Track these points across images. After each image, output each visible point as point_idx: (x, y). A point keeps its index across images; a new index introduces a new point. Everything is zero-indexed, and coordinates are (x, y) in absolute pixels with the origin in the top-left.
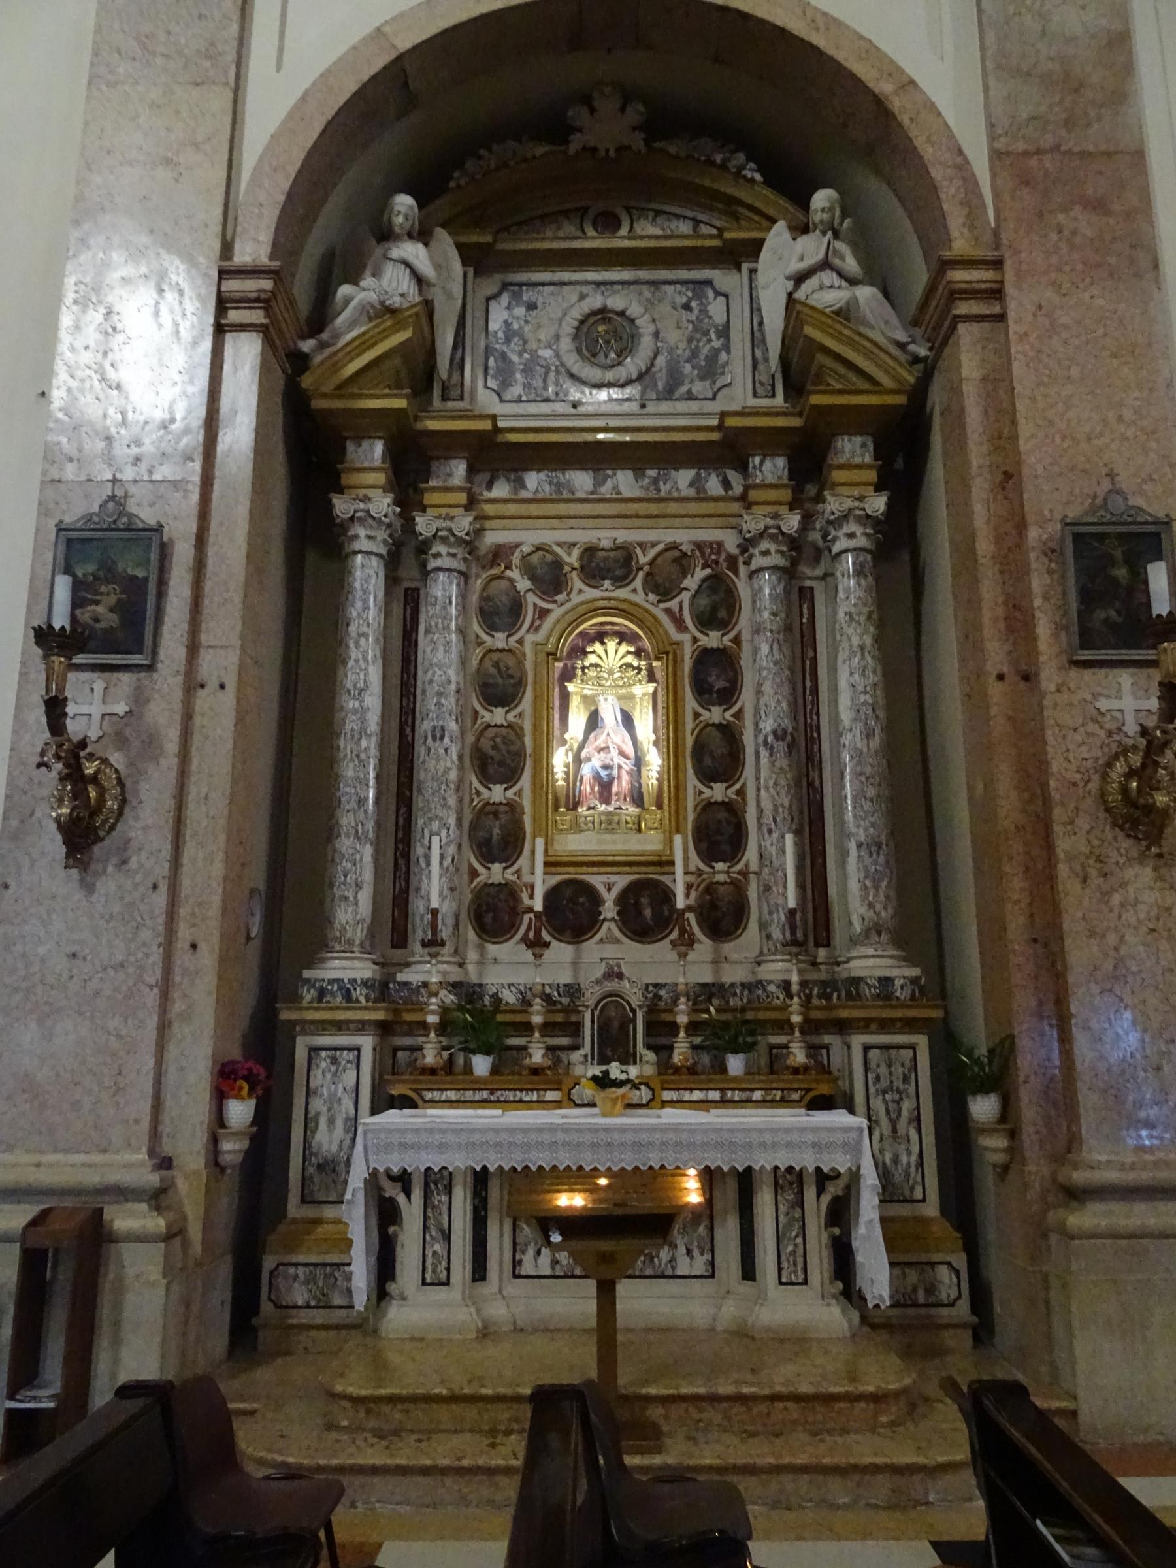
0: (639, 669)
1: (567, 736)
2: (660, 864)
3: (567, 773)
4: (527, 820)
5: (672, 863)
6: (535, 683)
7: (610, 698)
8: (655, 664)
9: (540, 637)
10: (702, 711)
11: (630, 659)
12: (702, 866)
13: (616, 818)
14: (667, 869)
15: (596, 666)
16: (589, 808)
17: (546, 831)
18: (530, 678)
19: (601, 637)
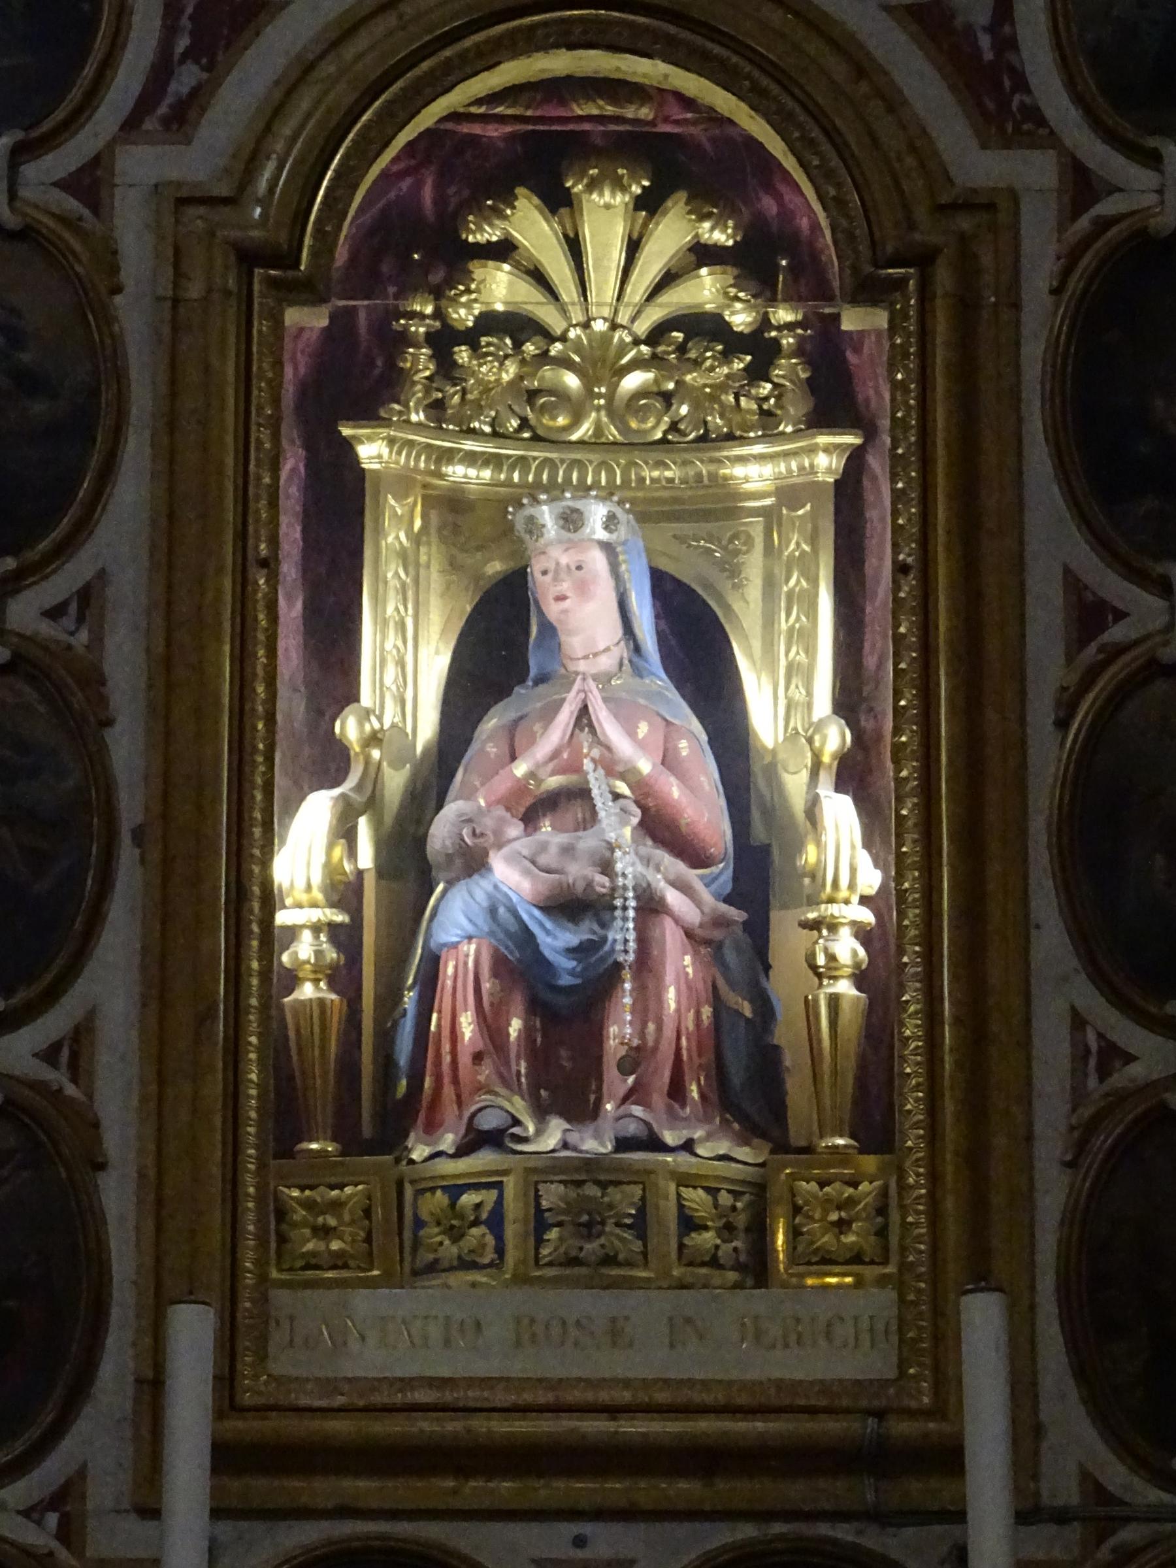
0: (760, 349)
1: (349, 728)
2: (878, 1459)
3: (345, 937)
4: (117, 1196)
5: (950, 1458)
6: (170, 421)
7: (597, 512)
8: (851, 320)
9: (198, 160)
10: (1112, 586)
11: (706, 289)
12: (1117, 1476)
13: (625, 1199)
14: (916, 1489)
15: (515, 326)
16: (475, 1140)
17: (229, 1261)
18: (142, 398)
19: (545, 164)
